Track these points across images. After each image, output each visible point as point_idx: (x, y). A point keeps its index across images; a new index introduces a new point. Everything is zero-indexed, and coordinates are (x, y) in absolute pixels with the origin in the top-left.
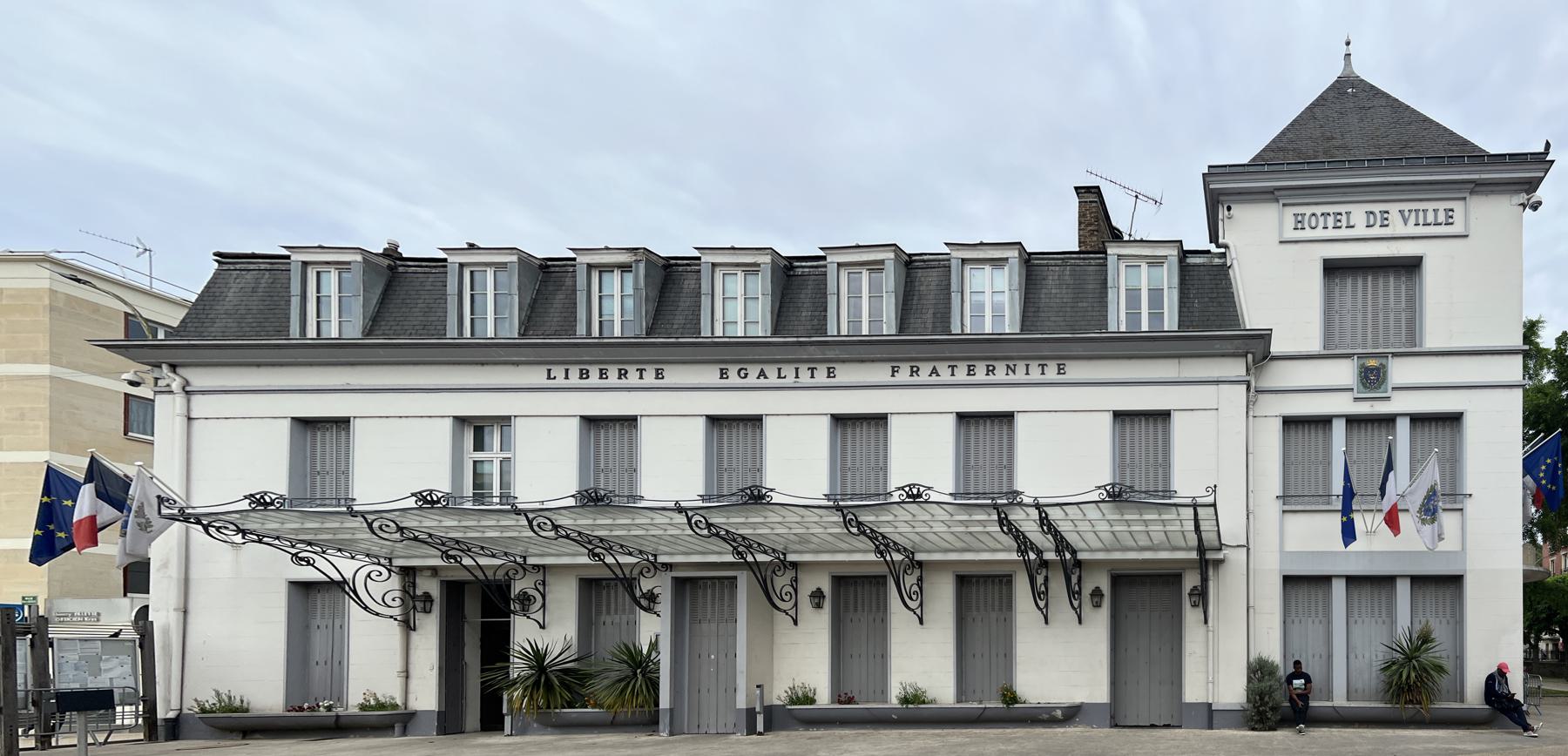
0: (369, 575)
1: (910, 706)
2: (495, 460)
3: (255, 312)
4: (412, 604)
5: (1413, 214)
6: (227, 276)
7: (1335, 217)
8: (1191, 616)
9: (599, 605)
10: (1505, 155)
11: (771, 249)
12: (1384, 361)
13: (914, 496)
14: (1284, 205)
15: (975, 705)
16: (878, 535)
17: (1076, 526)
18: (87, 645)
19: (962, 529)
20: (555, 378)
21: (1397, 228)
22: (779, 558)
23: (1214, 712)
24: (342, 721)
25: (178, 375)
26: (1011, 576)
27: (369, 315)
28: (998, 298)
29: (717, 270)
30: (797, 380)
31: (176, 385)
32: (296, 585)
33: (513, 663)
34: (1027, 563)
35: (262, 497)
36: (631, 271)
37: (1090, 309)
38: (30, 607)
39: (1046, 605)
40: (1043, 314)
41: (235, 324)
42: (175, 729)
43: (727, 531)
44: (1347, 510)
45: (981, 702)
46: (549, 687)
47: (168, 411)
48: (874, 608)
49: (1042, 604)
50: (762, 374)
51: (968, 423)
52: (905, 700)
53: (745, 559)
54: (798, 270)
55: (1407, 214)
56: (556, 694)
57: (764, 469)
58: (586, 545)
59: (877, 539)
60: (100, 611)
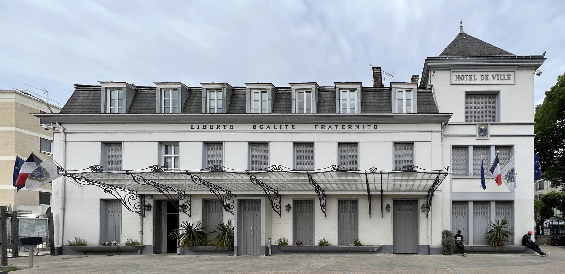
0: (130, 197)
1: (323, 246)
2: (172, 157)
3: (88, 105)
4: (144, 208)
5: (497, 76)
6: (79, 93)
7: (470, 77)
8: (422, 215)
9: (209, 208)
10: (530, 56)
11: (272, 83)
12: (487, 127)
13: (277, 169)
14: (453, 72)
15: (346, 246)
16: (264, 184)
17: (329, 182)
18: (30, 221)
19: (295, 182)
20: (194, 128)
21: (491, 81)
22: (228, 193)
23: (430, 249)
24: (120, 249)
25: (62, 126)
26: (313, 200)
27: (128, 106)
28: (352, 102)
29: (252, 91)
30: (281, 129)
31: (61, 130)
32: (103, 201)
33: (180, 229)
34: (319, 195)
35: (96, 167)
36: (221, 91)
37: (385, 106)
38: (8, 208)
39: (326, 211)
40: (368, 108)
41: (82, 109)
42: (61, 251)
43: (208, 183)
44: (483, 178)
45: (347, 245)
46: (194, 237)
47: (58, 139)
48: (308, 212)
49: (324, 210)
50: (268, 127)
51: (297, 146)
52: (321, 244)
53: (267, 193)
54: (280, 92)
55: (494, 76)
56: (196, 240)
57: (224, 161)
58: (157, 187)
59: (264, 186)
60: (32, 210)
